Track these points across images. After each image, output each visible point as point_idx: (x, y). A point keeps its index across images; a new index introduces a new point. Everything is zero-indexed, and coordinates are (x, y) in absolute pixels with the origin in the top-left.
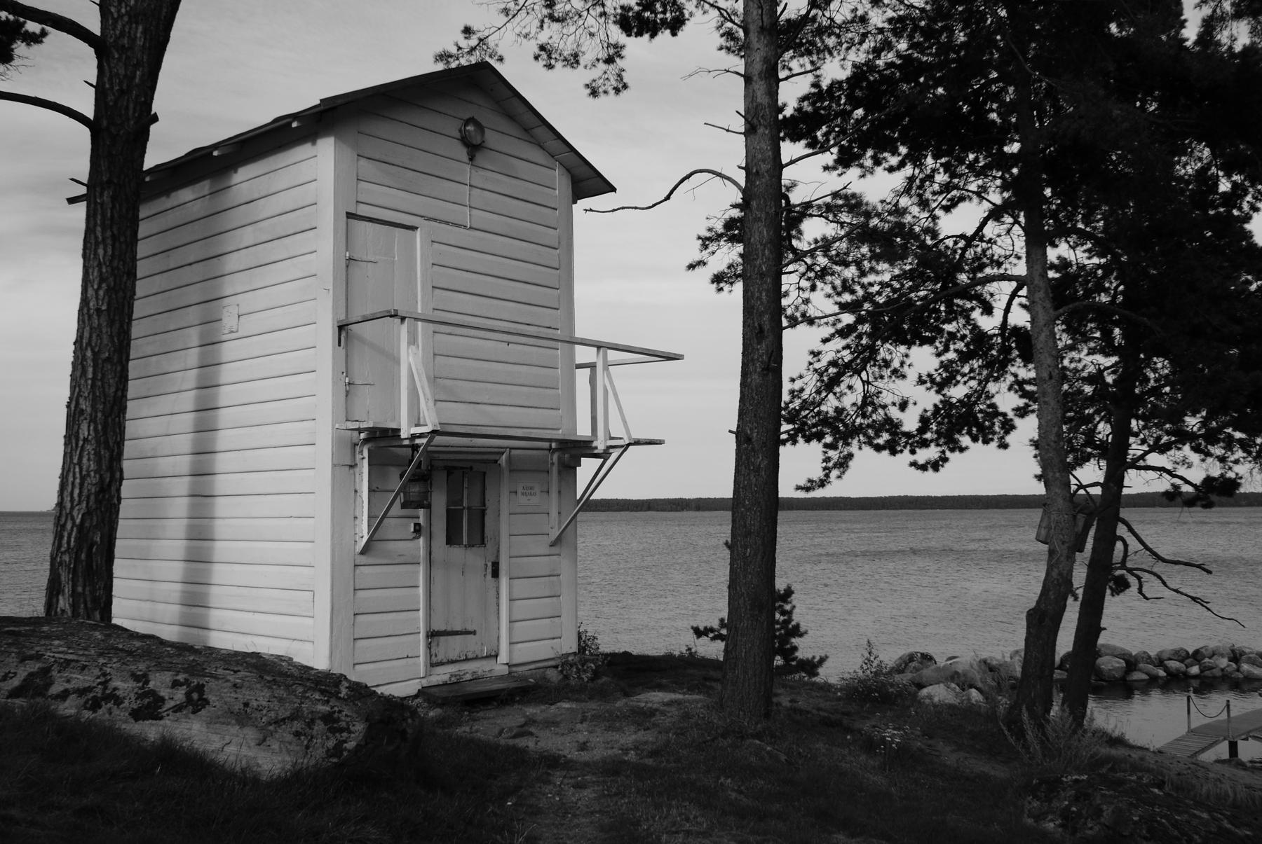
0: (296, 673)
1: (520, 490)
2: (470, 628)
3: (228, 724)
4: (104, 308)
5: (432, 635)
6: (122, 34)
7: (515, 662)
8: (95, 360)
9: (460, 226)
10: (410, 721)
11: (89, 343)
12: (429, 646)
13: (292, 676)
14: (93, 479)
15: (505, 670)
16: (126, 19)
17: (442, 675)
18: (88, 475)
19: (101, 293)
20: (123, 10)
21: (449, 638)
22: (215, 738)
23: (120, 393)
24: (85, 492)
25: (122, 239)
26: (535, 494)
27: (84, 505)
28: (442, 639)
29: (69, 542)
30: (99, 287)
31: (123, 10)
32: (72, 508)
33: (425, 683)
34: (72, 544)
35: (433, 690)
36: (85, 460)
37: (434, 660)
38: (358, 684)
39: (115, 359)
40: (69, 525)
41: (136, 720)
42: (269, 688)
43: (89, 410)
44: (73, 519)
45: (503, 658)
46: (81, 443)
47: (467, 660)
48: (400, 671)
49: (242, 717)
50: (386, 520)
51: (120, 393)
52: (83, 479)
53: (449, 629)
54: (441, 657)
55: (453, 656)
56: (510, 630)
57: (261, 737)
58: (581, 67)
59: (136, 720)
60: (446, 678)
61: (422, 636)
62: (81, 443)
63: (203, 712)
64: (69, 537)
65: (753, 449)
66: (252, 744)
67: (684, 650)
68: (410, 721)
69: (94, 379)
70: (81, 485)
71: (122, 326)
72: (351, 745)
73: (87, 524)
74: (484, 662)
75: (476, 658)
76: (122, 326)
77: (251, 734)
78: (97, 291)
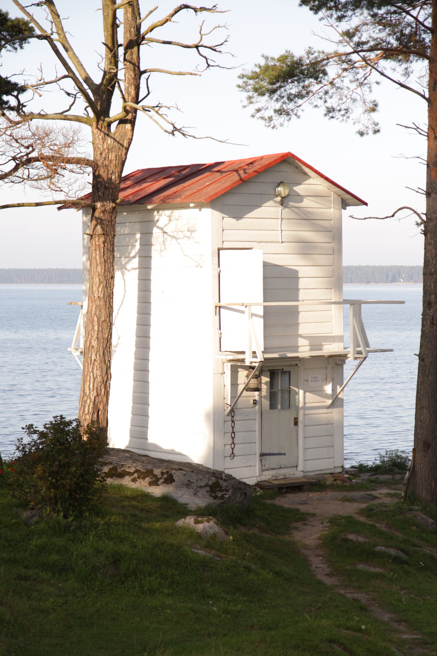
0: (205, 470)
1: (310, 379)
2: (282, 452)
3: (183, 488)
4: (102, 296)
5: (262, 455)
6: (105, 158)
7: (306, 470)
8: (98, 322)
9: (275, 242)
10: (248, 489)
11: (95, 314)
12: (261, 461)
13: (204, 471)
14: (99, 379)
15: (302, 474)
16: (107, 151)
17: (267, 476)
18: (97, 377)
19: (100, 289)
20: (105, 146)
21: (272, 456)
22: (179, 492)
23: (110, 337)
24: (96, 386)
25: (109, 261)
26: (318, 381)
27: (95, 391)
28: (267, 457)
29: (88, 410)
30: (99, 286)
31: (105, 146)
32: (90, 393)
33: (259, 479)
34: (90, 410)
35: (262, 483)
36: (95, 371)
37: (264, 468)
38: (229, 475)
39: (108, 320)
40: (88, 401)
41: (150, 486)
42: (197, 475)
43: (96, 346)
44: (90, 398)
45: (300, 468)
46: (93, 362)
47: (280, 468)
48: (248, 471)
49: (188, 485)
50: (240, 398)
51: (110, 337)
52: (94, 379)
53: (271, 452)
54: (267, 467)
55: (273, 467)
56: (304, 453)
57: (195, 492)
58: (350, 121)
59: (150, 486)
60: (270, 477)
61: (258, 455)
62: (93, 362)
63: (173, 483)
64: (89, 407)
65: (425, 365)
66: (192, 495)
67: (52, 419)
68: (248, 489)
69: (98, 331)
70: (94, 382)
71: (110, 304)
72: (226, 496)
73: (97, 401)
74: (290, 470)
75: (286, 467)
76: (110, 304)
77: (191, 491)
78: (98, 289)
